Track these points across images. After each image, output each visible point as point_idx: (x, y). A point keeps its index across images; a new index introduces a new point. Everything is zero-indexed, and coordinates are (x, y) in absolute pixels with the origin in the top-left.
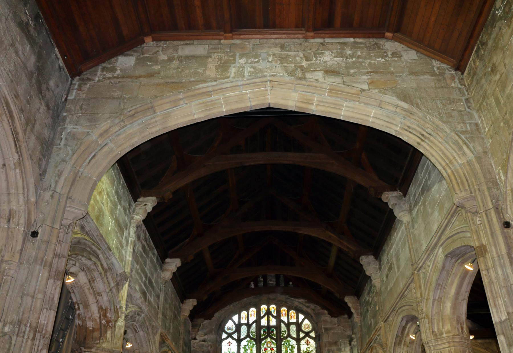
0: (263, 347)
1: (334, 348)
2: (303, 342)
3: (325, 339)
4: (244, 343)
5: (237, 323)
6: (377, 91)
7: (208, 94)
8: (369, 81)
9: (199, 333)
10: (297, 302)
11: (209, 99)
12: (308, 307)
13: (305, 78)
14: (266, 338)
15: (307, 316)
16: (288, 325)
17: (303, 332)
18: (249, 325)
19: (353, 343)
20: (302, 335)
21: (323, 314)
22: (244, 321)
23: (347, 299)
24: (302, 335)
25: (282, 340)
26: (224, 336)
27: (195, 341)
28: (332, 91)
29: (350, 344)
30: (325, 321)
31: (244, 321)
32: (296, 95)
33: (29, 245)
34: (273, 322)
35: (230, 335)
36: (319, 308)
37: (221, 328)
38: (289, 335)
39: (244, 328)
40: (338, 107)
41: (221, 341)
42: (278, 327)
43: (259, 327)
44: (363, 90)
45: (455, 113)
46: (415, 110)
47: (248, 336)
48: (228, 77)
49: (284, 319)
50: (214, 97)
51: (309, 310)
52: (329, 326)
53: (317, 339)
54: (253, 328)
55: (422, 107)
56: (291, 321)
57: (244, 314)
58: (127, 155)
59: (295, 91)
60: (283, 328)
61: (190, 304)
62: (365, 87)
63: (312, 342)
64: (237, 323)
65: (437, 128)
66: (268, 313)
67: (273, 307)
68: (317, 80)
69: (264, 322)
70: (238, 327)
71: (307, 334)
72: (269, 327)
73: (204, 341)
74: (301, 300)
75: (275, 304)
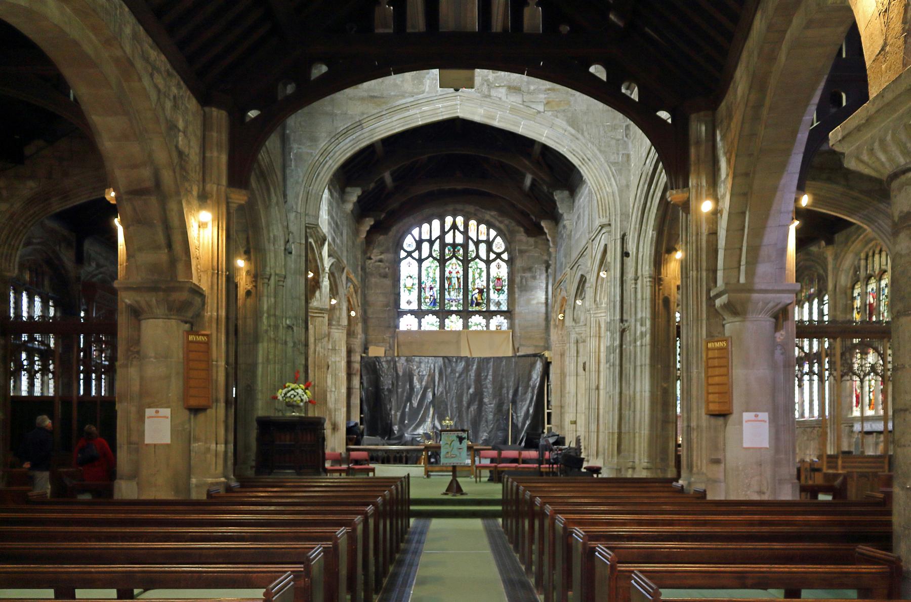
0: (447, 270)
1: (528, 275)
2: (493, 266)
3: (519, 263)
4: (425, 264)
5: (417, 239)
6: (550, 113)
7: (406, 108)
8: (545, 102)
9: (375, 251)
10: (488, 215)
11: (407, 114)
12: (501, 222)
13: (489, 96)
14: (450, 258)
15: (500, 233)
16: (477, 243)
17: (495, 253)
18: (431, 242)
19: (549, 270)
20: (492, 256)
21: (518, 232)
22: (425, 236)
23: (543, 224)
24: (492, 256)
25: (469, 262)
26: (403, 254)
27: (370, 261)
28: (513, 110)
29: (547, 271)
30: (520, 241)
31: (425, 236)
32: (481, 111)
33: (288, 259)
34: (460, 239)
35: (409, 254)
36: (513, 224)
37: (399, 246)
38: (478, 256)
39: (426, 246)
40: (517, 124)
41: (400, 260)
42: (465, 246)
43: (443, 245)
44: (539, 112)
45: (613, 142)
46: (579, 136)
47: (431, 255)
48: (423, 92)
49: (472, 234)
50: (411, 112)
51: (502, 226)
52: (523, 248)
53: (510, 262)
54: (436, 246)
55: (586, 134)
56: (480, 238)
57: (426, 227)
58: (388, 282)
59: (481, 106)
60: (472, 247)
61: (369, 222)
62: (541, 108)
63: (504, 266)
64: (417, 239)
65: (595, 155)
66: (454, 227)
67: (460, 220)
68: (500, 99)
69: (449, 239)
70: (419, 243)
71: (499, 256)
72: (454, 245)
73: (381, 261)
74: (493, 213)
75: (463, 216)
